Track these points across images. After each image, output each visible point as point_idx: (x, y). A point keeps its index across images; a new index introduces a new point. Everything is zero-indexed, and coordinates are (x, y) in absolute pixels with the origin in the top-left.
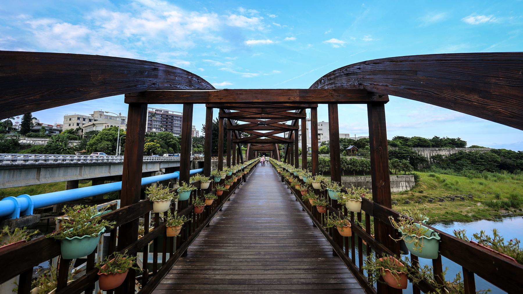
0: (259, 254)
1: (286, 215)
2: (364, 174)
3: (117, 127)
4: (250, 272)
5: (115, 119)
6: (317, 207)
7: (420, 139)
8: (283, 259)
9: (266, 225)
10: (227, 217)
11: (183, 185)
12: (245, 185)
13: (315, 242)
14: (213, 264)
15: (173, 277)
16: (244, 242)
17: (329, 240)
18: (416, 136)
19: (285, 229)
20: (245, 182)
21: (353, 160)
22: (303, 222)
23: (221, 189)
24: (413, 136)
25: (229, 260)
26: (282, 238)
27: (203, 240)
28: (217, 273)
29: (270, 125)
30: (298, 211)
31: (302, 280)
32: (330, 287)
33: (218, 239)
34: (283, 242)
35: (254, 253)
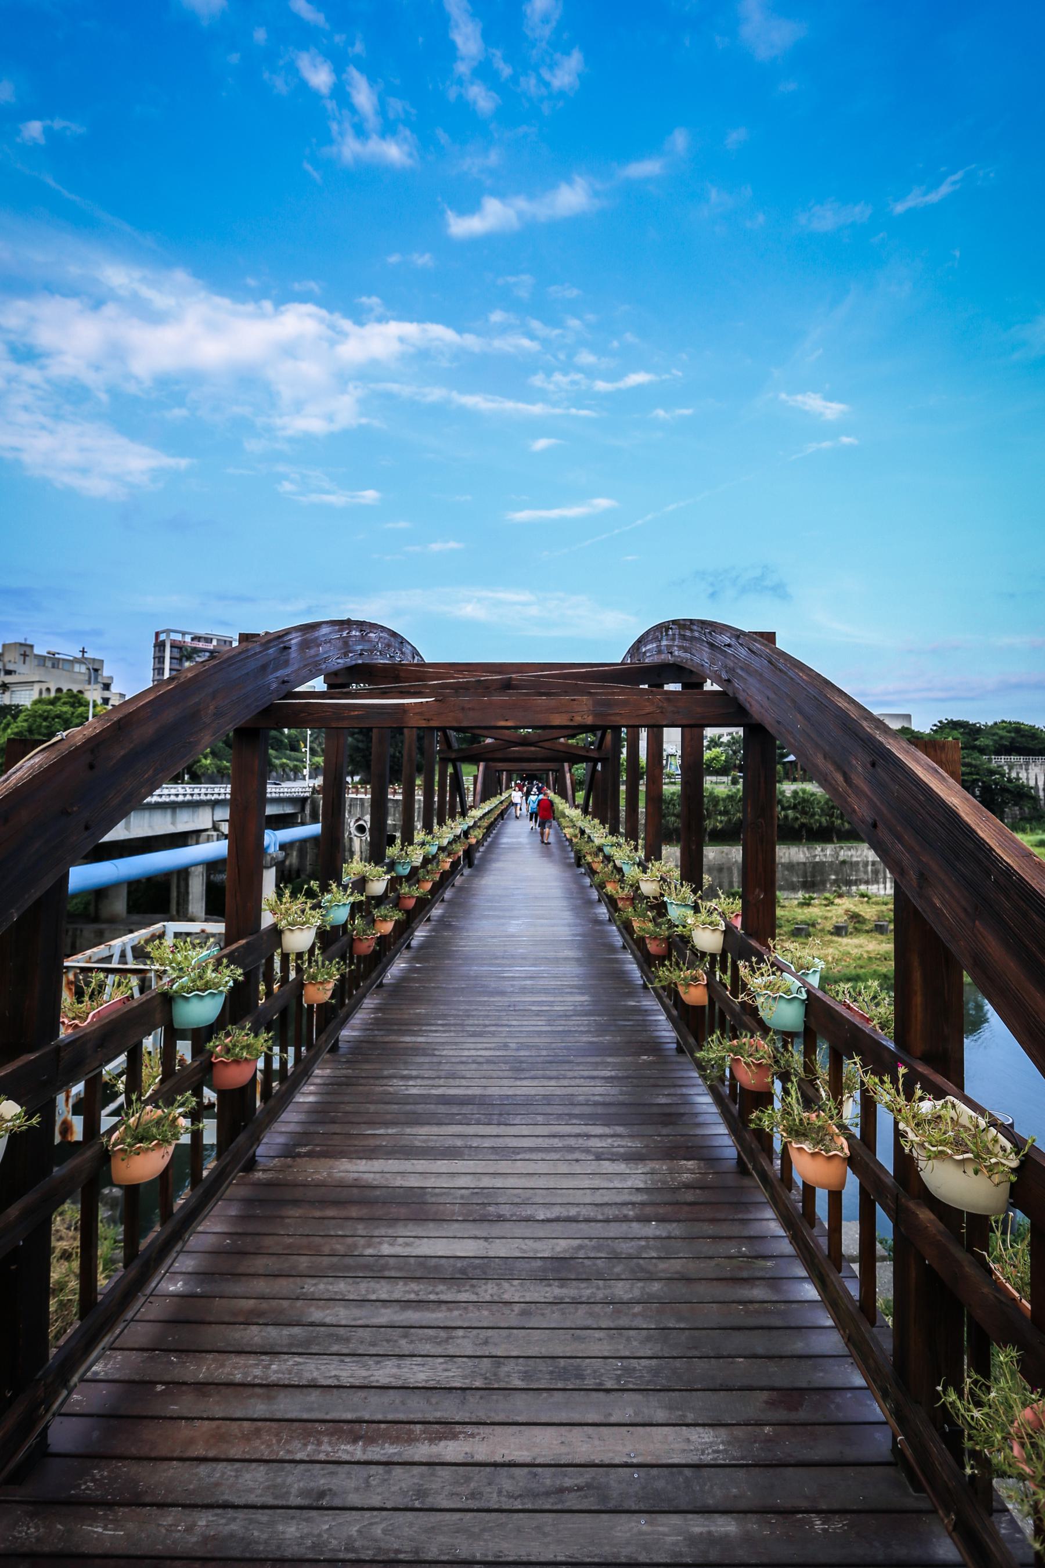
0: (505, 1046)
1: (578, 960)
2: (835, 840)
3: (75, 691)
4: (484, 1082)
5: (67, 666)
6: (647, 941)
7: (1017, 729)
8: (560, 1058)
9: (524, 983)
10: (427, 964)
11: (909, 1097)
12: (470, 876)
13: (641, 1023)
14: (402, 1066)
15: (316, 1091)
16: (471, 1022)
17: (670, 1017)
18: (1007, 720)
19: (571, 993)
20: (470, 866)
21: (801, 794)
22: (620, 976)
23: (412, 892)
24: (999, 720)
25: (435, 1059)
26: (561, 1013)
27: (371, 1019)
28: (411, 1083)
29: (541, 744)
30: (612, 949)
31: (597, 1098)
32: (655, 1110)
33: (406, 1017)
34: (563, 1022)
35: (494, 1045)
